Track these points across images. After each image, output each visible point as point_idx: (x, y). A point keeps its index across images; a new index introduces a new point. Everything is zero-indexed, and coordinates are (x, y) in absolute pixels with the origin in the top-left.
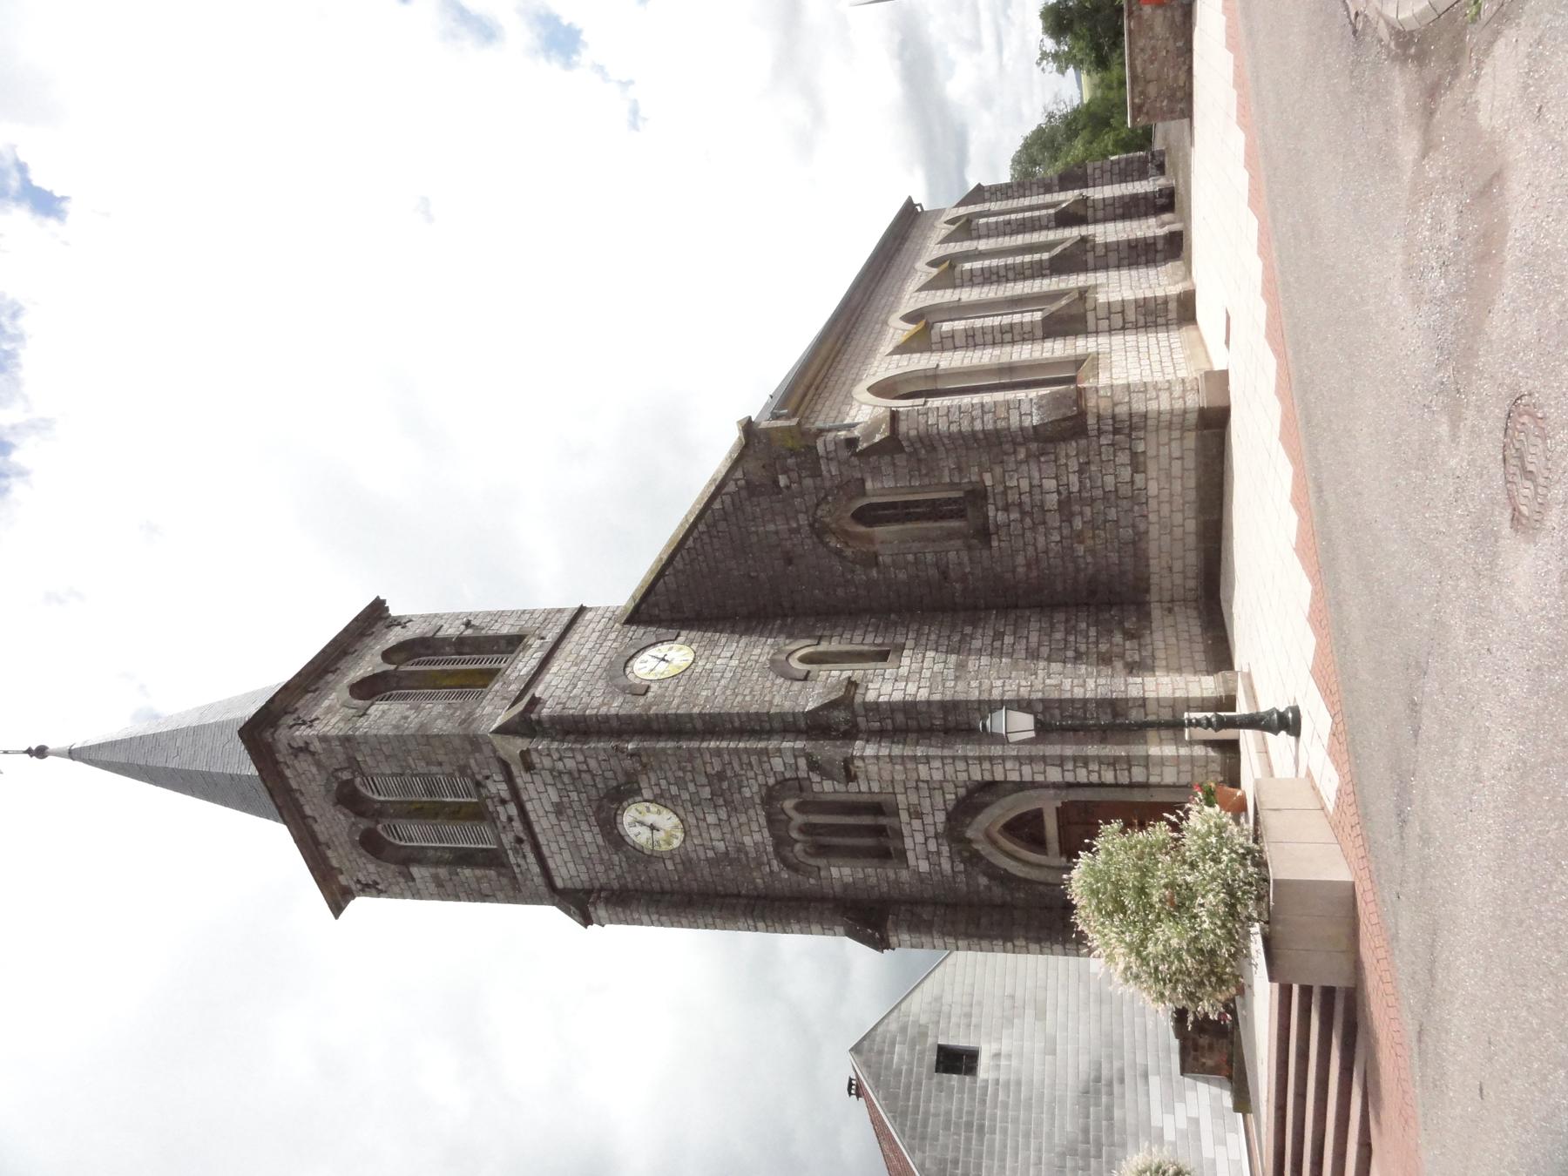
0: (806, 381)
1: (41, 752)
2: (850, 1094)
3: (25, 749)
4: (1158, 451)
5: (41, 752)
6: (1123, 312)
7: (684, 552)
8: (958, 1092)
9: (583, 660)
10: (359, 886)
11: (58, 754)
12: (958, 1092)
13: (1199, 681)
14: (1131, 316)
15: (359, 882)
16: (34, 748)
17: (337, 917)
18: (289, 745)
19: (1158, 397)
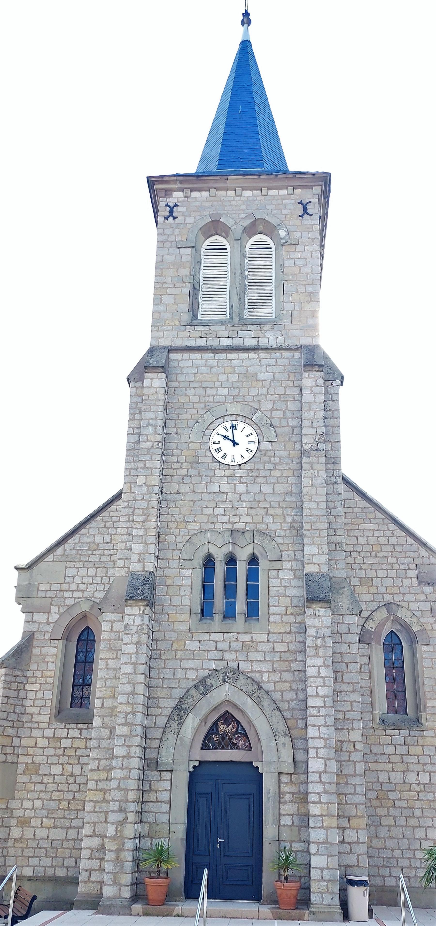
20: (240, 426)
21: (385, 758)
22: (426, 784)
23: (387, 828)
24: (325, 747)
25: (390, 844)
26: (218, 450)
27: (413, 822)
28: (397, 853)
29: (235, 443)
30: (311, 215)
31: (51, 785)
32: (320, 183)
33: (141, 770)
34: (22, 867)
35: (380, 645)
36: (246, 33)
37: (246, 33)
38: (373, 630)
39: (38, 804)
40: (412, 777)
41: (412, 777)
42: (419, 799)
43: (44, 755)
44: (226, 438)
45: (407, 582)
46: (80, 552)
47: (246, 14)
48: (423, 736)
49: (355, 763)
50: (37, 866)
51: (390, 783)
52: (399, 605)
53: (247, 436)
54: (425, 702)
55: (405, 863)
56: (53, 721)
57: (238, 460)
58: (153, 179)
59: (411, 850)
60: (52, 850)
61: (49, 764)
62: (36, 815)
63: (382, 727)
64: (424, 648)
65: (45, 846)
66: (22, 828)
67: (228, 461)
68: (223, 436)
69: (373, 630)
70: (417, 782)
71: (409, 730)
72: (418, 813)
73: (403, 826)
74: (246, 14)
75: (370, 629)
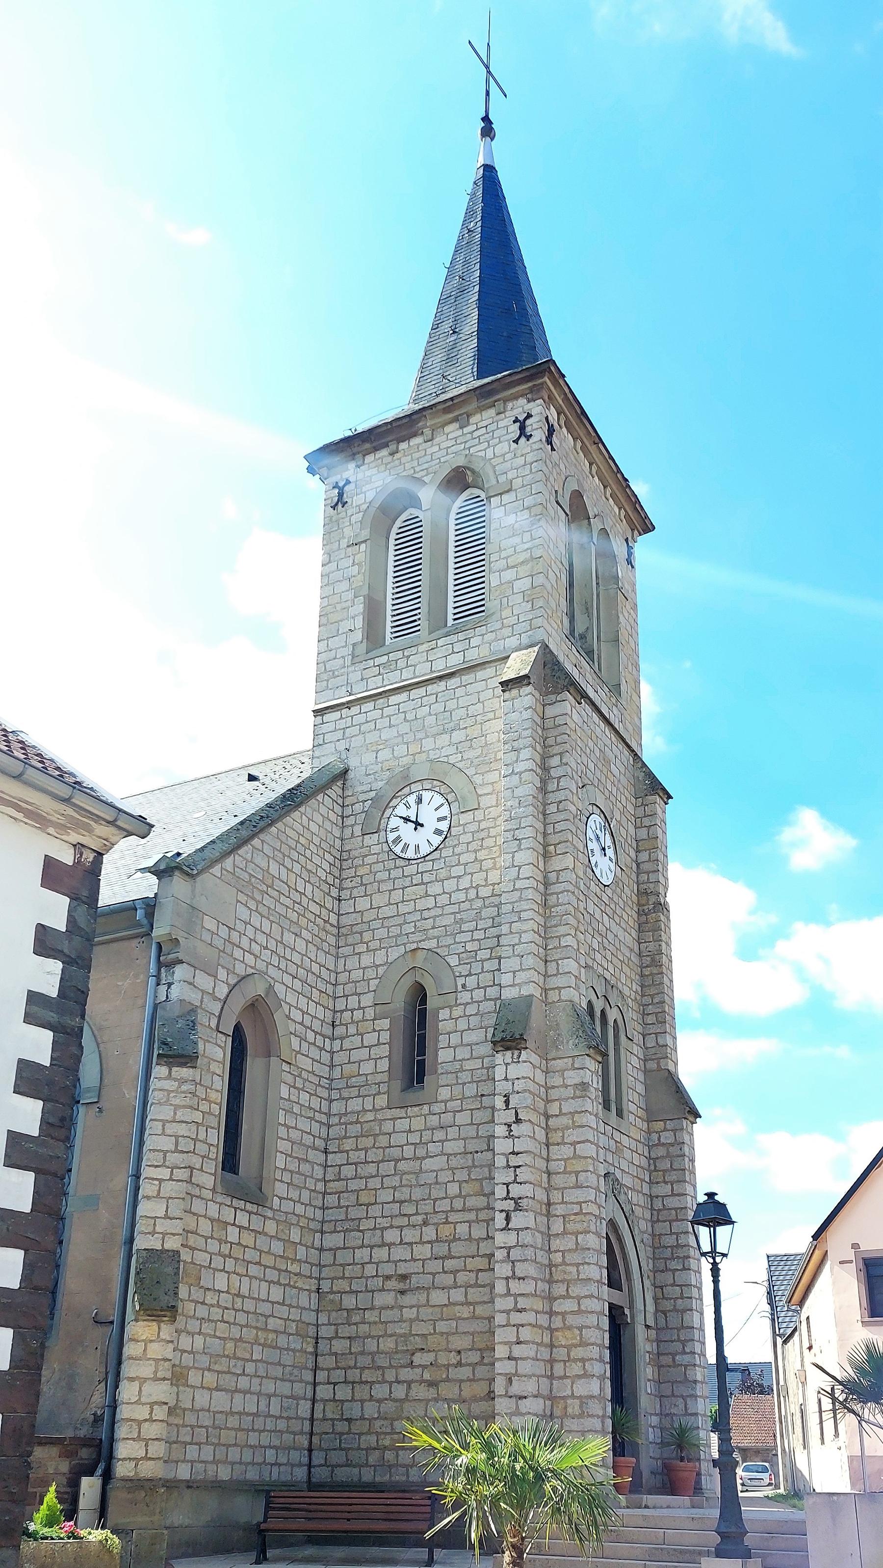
20: (426, 796)
26: (398, 840)
29: (418, 824)
30: (516, 442)
33: (307, 1383)
34: (177, 1462)
36: (489, 153)
37: (489, 153)
39: (199, 1341)
43: (206, 1251)
44: (407, 820)
46: (253, 880)
47: (486, 119)
50: (195, 1461)
53: (436, 809)
56: (219, 1189)
57: (425, 849)
58: (552, 368)
60: (214, 1431)
61: (213, 1269)
62: (196, 1365)
65: (206, 1424)
66: (177, 1386)
67: (410, 854)
68: (404, 818)
74: (486, 119)
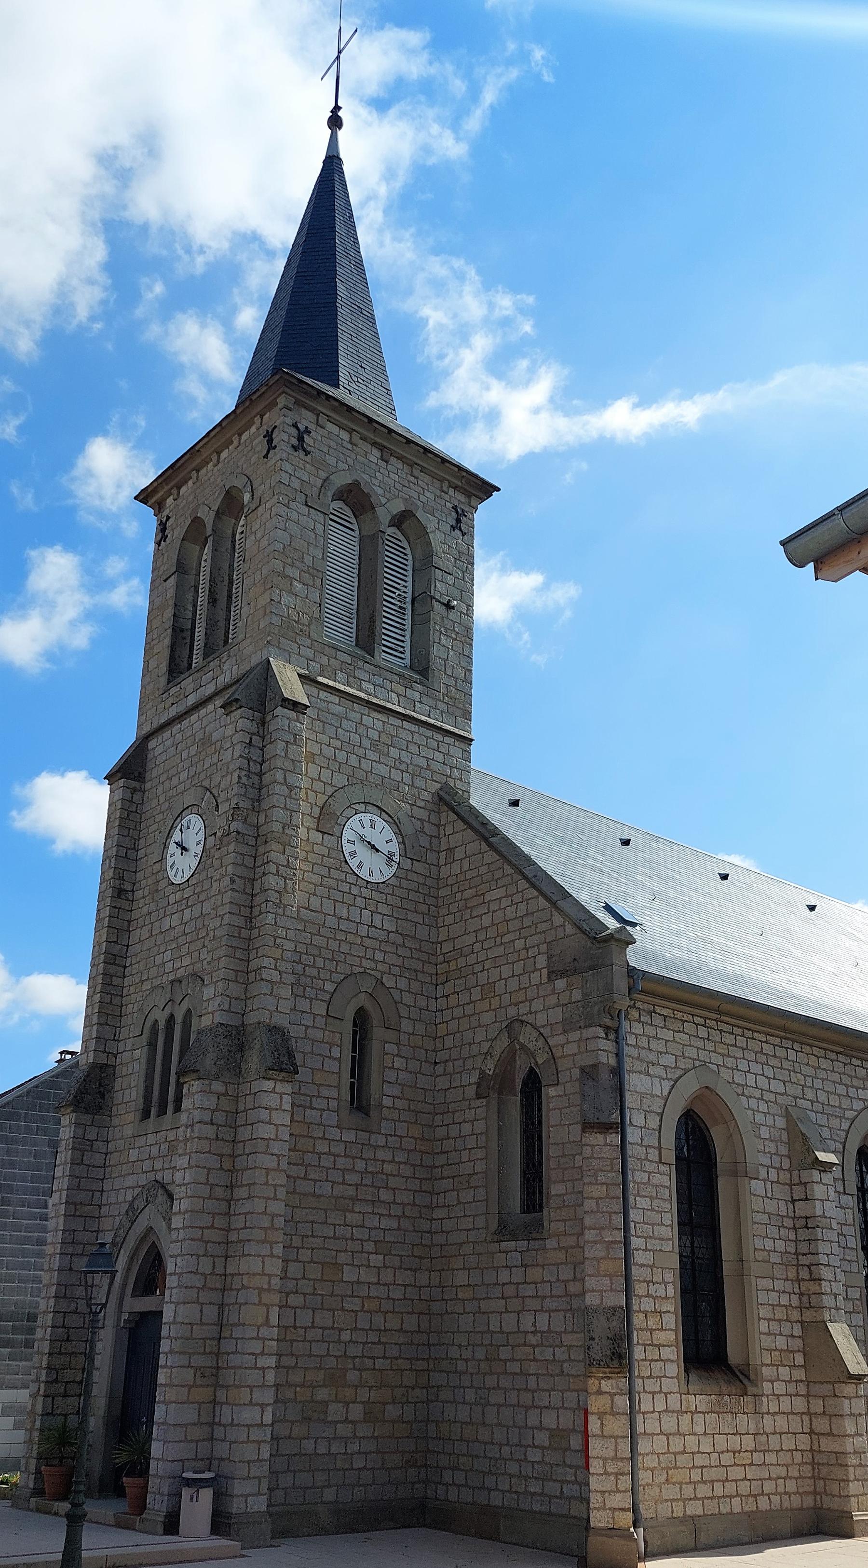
0: (725, 1007)
1: (335, 122)
2: (61, 1053)
3: (340, 104)
4: (570, 1467)
5: (335, 122)
6: (830, 1434)
7: (499, 863)
8: (33, 1175)
9: (380, 753)
10: (164, 520)
11: (333, 142)
12: (33, 1175)
13: (259, 1494)
14: (826, 1444)
15: (168, 518)
16: (340, 114)
17: (136, 498)
18: (276, 427)
19: (606, 1473)
21: (497, 1292)
22: (544, 1332)
23: (495, 1409)
24: (179, 1286)
25: (499, 1436)
27: (526, 1399)
28: (506, 1450)
31: (300, 1345)
32: (280, 391)
35: (515, 1095)
38: (491, 1073)
40: (527, 1322)
41: (527, 1322)
42: (535, 1360)
45: (535, 978)
48: (544, 1249)
49: (268, 1306)
51: (501, 1332)
52: (522, 1022)
54: (548, 1188)
55: (513, 1468)
59: (521, 1446)
63: (495, 1238)
64: (552, 1091)
69: (491, 1073)
70: (533, 1329)
71: (528, 1240)
72: (532, 1382)
73: (514, 1406)
75: (488, 1072)
